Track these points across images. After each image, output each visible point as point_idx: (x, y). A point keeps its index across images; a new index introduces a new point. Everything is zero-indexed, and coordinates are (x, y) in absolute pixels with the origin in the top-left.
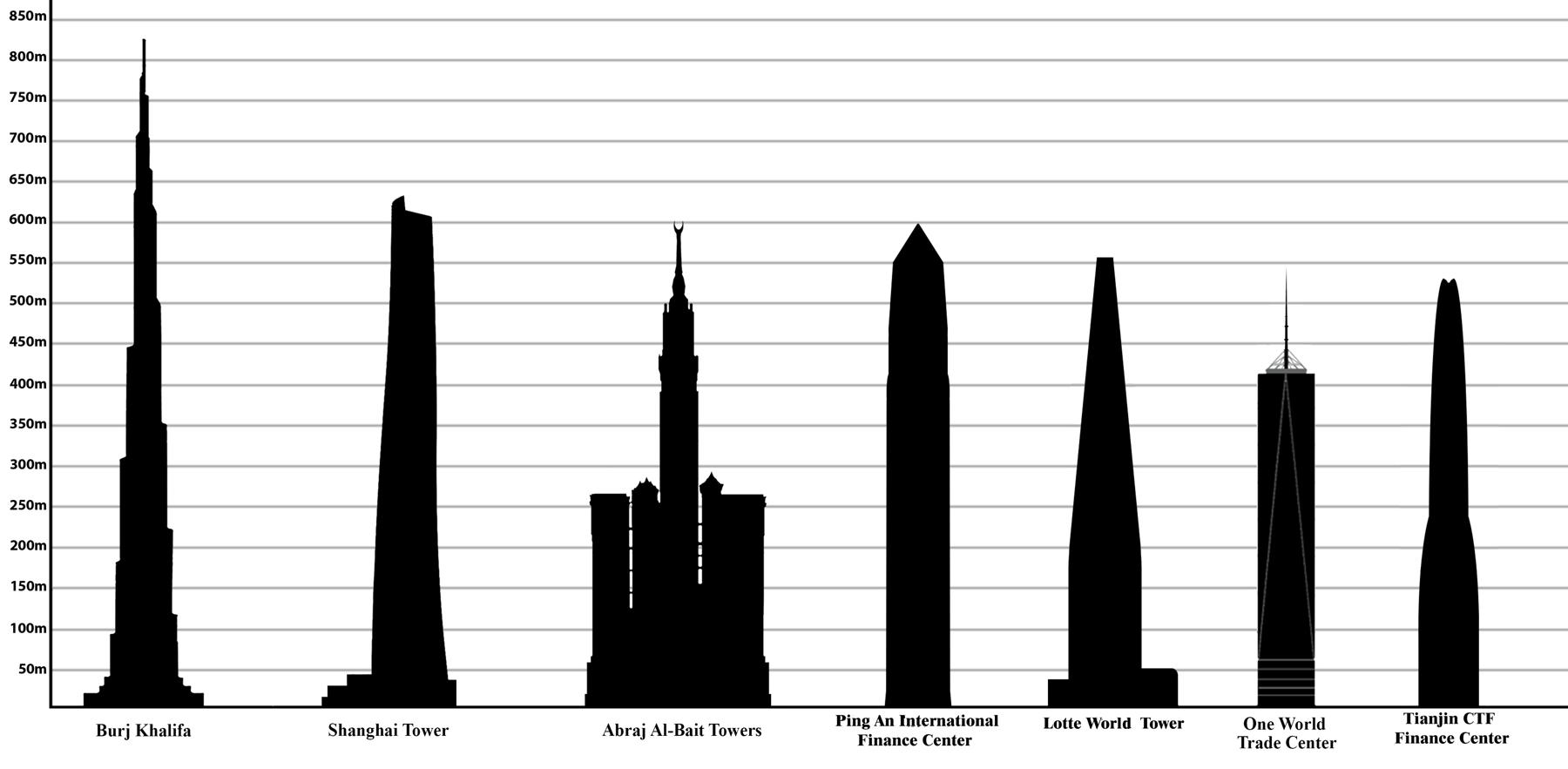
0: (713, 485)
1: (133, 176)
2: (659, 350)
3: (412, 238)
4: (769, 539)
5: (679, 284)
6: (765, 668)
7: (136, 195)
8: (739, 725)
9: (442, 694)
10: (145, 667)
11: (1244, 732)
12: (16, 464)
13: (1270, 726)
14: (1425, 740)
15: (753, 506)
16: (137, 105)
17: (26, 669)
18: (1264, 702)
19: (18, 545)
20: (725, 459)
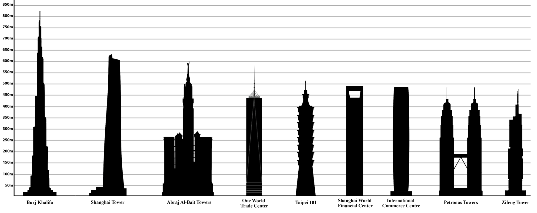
0: (198, 134)
1: (37, 49)
2: (183, 97)
3: (114, 66)
4: (213, 149)
5: (188, 79)
6: (212, 185)
7: (38, 54)
8: (205, 201)
9: (123, 192)
10: (40, 185)
11: (242, 203)
12: (4, 129)
13: (249, 201)
14: (346, 206)
15: (209, 140)
16: (38, 29)
17: (7, 185)
18: (248, 195)
19: (5, 151)
20: (201, 127)
